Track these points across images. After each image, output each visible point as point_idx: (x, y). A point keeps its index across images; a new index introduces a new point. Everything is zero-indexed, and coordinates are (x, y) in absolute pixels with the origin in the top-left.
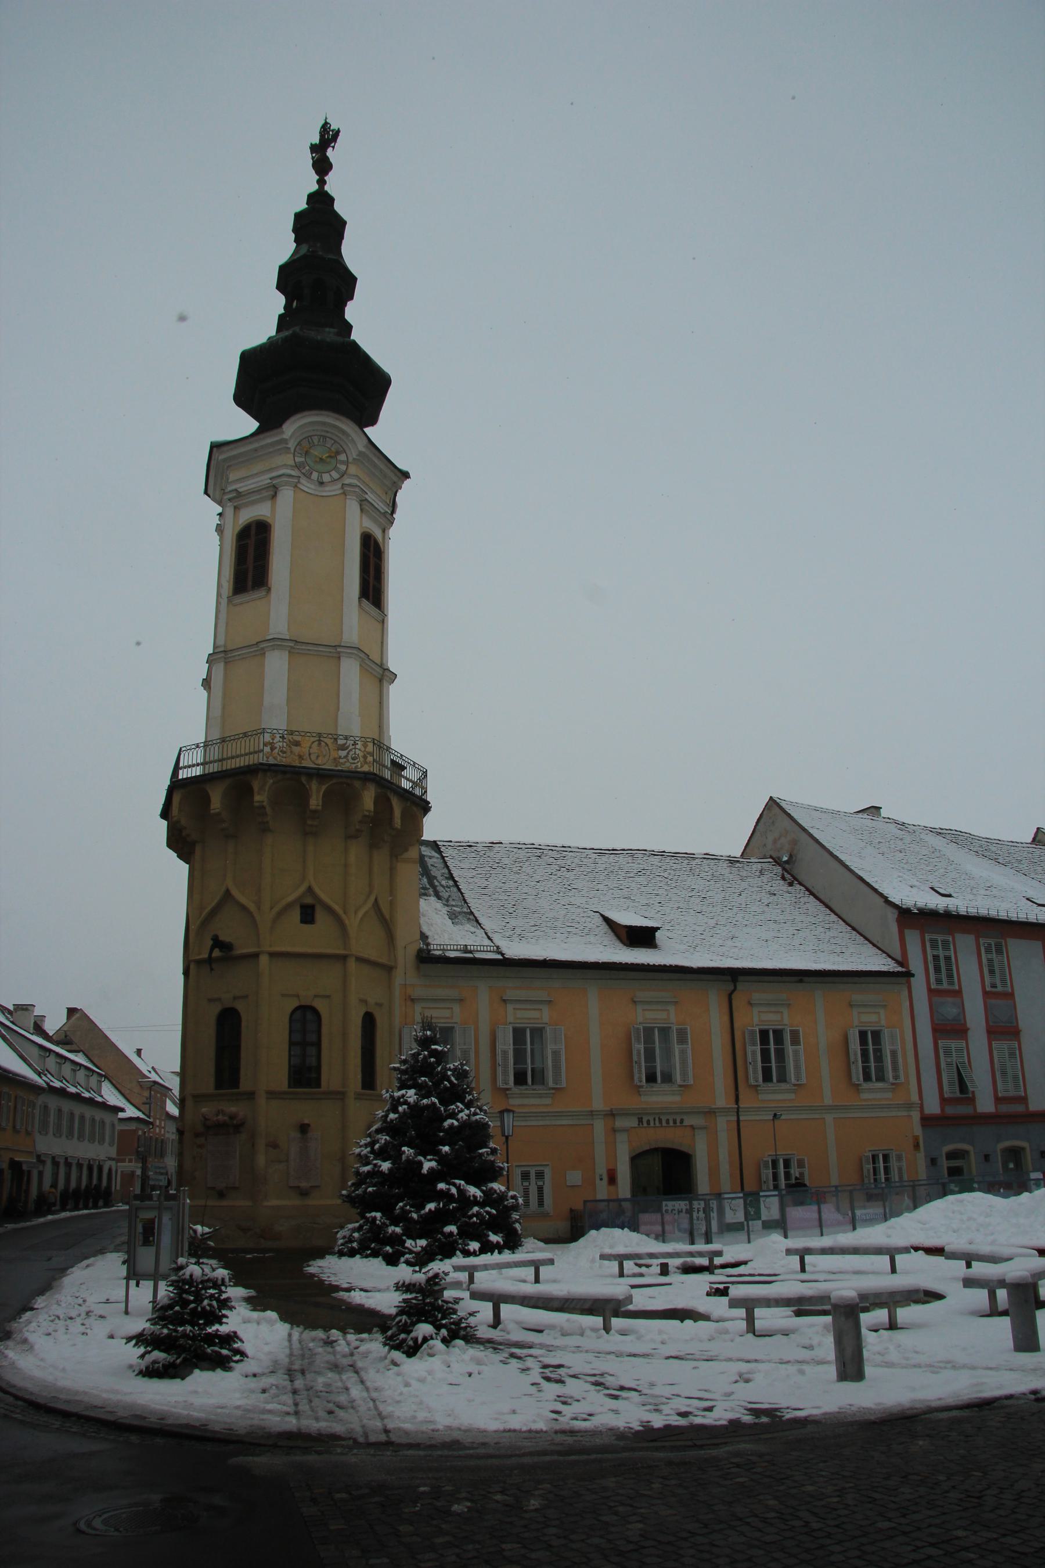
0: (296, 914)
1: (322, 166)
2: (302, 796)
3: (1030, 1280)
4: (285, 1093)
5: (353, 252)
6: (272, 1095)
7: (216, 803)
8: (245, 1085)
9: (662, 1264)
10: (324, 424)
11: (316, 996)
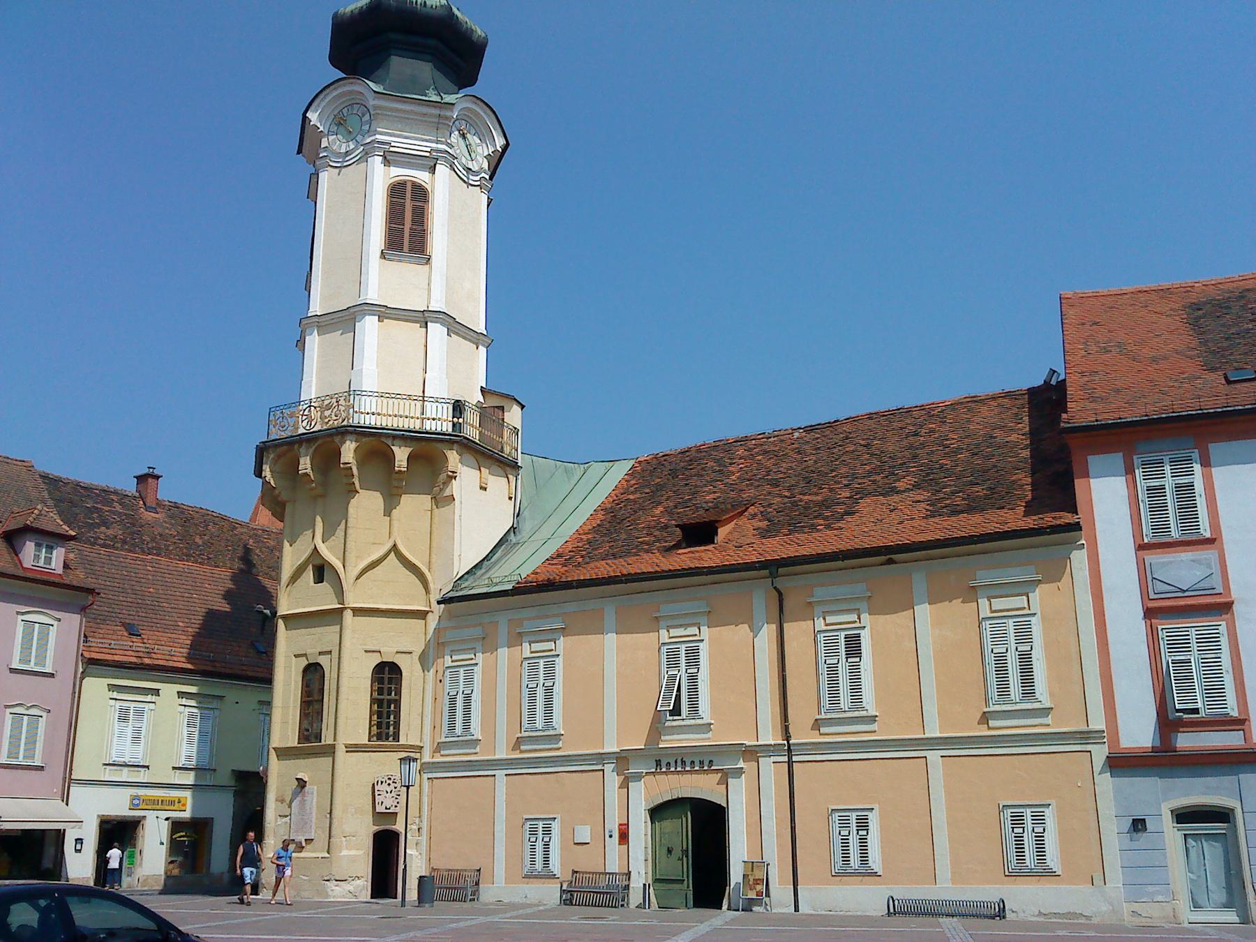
0: (309, 574)
3: (63, 874)
4: (365, 746)
6: (353, 749)
7: (305, 464)
8: (327, 739)
9: (257, 894)
10: (351, 92)
11: (320, 653)
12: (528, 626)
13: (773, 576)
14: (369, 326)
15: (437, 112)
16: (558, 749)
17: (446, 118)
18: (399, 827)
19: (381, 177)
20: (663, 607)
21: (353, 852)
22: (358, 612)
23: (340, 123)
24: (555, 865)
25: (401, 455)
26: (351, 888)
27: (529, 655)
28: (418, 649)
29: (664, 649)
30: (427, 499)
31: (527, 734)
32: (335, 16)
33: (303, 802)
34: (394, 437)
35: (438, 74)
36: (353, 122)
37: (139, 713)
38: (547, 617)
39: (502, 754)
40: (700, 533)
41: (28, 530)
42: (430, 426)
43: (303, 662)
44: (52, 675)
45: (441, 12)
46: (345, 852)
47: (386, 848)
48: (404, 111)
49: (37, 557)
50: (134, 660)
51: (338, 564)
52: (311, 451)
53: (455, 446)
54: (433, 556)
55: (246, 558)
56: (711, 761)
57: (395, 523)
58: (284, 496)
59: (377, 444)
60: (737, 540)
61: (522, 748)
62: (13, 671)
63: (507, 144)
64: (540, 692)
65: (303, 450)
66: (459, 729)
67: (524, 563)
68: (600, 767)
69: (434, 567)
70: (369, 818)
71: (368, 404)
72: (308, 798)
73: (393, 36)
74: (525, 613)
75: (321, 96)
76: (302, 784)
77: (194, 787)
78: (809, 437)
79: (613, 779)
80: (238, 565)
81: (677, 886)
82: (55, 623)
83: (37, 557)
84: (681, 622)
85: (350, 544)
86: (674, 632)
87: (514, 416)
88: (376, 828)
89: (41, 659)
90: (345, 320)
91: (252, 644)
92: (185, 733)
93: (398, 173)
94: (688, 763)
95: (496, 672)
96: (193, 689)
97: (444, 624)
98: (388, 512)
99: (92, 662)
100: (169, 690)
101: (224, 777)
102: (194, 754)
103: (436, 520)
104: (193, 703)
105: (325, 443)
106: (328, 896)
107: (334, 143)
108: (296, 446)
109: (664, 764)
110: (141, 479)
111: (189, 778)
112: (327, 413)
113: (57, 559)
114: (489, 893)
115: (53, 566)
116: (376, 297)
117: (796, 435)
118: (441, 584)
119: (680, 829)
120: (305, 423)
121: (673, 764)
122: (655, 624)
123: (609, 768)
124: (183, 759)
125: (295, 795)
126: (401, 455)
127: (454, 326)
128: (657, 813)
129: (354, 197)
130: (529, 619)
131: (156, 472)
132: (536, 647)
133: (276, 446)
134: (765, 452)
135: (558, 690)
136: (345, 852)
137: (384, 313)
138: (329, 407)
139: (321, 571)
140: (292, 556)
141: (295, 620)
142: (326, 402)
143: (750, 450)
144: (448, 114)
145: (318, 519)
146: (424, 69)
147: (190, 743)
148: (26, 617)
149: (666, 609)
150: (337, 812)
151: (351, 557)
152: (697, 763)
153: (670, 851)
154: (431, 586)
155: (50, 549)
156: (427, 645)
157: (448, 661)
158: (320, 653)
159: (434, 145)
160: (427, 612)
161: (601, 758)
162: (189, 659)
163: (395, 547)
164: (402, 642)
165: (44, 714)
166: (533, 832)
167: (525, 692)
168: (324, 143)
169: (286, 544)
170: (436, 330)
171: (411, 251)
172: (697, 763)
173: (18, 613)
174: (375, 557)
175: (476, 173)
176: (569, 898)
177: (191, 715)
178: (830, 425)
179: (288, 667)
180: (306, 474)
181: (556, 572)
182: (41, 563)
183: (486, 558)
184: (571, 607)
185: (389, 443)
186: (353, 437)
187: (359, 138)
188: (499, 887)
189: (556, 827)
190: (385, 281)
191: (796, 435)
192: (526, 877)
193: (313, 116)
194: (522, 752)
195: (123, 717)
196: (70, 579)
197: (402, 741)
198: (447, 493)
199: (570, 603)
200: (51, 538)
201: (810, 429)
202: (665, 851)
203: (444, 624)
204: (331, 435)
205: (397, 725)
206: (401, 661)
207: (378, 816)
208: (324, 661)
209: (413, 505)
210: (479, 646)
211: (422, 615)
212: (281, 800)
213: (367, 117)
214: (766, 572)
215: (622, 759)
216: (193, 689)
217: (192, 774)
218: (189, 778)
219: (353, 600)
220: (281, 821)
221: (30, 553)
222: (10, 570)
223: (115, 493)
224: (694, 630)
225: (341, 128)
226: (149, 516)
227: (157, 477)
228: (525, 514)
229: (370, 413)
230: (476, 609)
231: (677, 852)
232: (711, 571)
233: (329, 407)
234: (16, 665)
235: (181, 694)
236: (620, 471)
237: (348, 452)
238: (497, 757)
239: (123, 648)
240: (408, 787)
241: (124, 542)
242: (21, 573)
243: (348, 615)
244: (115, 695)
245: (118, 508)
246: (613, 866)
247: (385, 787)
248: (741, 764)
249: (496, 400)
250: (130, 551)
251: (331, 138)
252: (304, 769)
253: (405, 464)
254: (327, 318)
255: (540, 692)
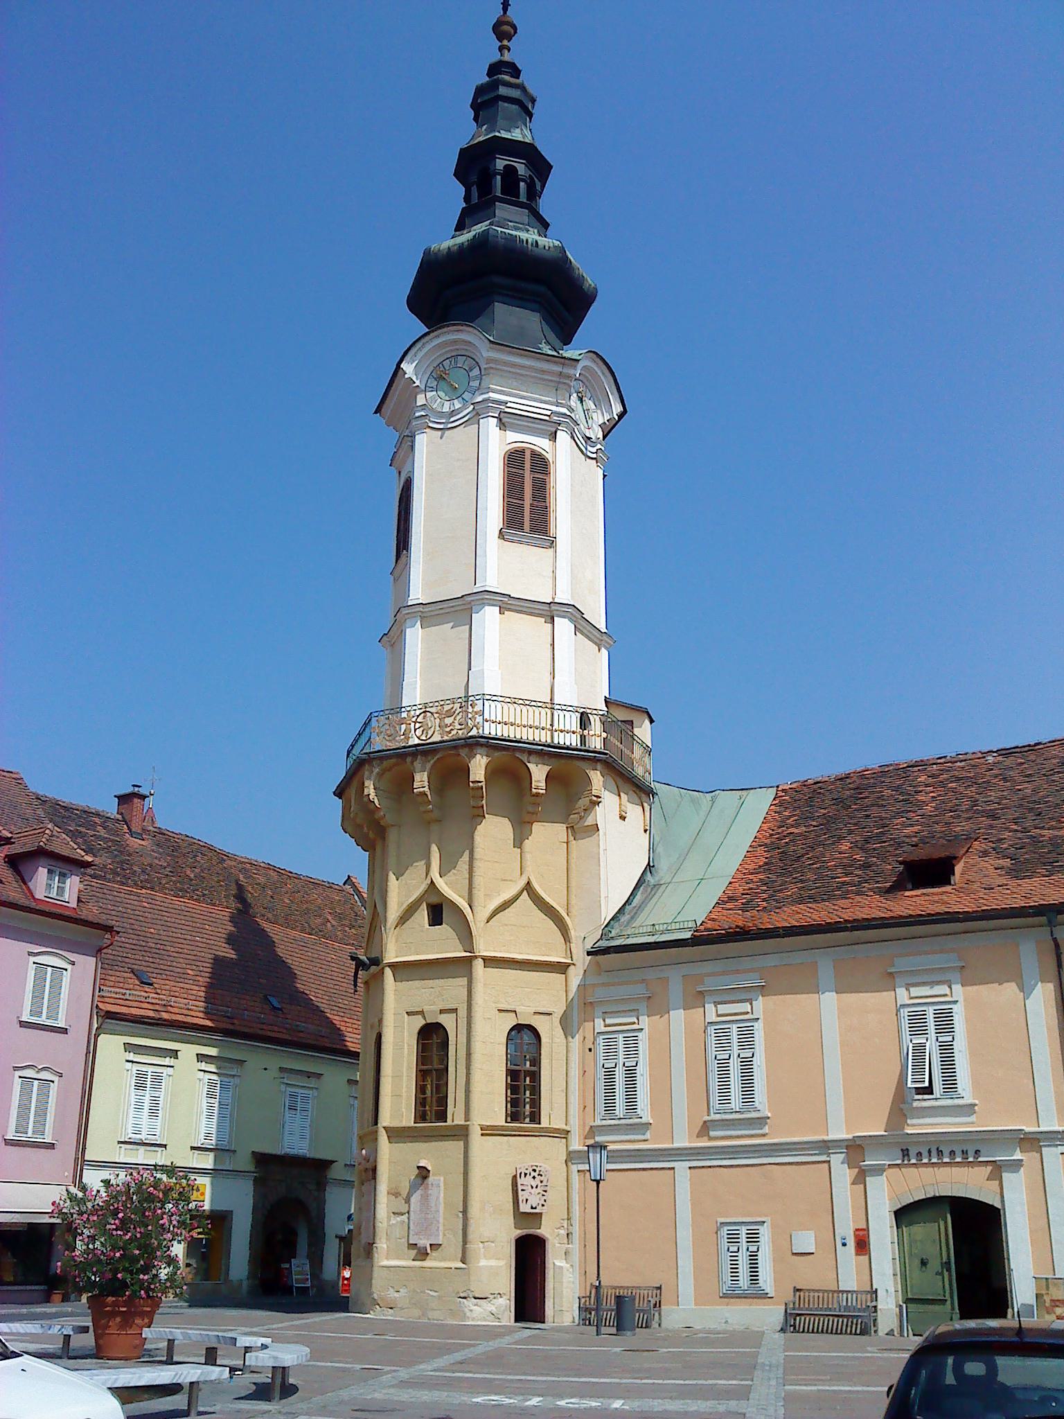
0: (423, 915)
1: (503, 31)
2: (519, 778)
5: (472, 114)
7: (421, 781)
8: (455, 1116)
10: (455, 342)
11: (442, 1012)
12: (710, 984)
13: (1051, 924)
14: (488, 617)
15: (558, 369)
16: (764, 1135)
17: (569, 377)
18: (544, 1231)
19: (496, 442)
20: (897, 961)
21: (493, 1263)
22: (490, 962)
23: (440, 377)
24: (766, 1279)
25: (539, 773)
26: (493, 1309)
27: (715, 1019)
28: (559, 1009)
29: (905, 1012)
30: (561, 828)
31: (718, 1117)
32: (427, 253)
33: (425, 1198)
34: (530, 752)
35: (546, 327)
36: (457, 378)
37: (157, 1079)
38: (737, 972)
39: (682, 1142)
40: (931, 871)
41: (41, 854)
42: (561, 739)
43: (419, 1022)
44: (64, 1031)
45: (556, 254)
46: (483, 1263)
47: (530, 1255)
48: (523, 367)
49: (49, 886)
50: (151, 1014)
51: (462, 903)
52: (429, 766)
53: (599, 766)
54: (573, 897)
55: (240, 896)
56: (977, 1152)
57: (528, 857)
58: (389, 819)
59: (510, 758)
60: (979, 880)
61: (712, 1133)
62: (23, 1024)
63: (625, 412)
64: (735, 1068)
65: (417, 764)
66: (620, 1109)
67: (687, 905)
68: (824, 1158)
69: (574, 911)
70: (510, 1220)
71: (493, 711)
72: (432, 1191)
73: (497, 279)
74: (708, 967)
75: (419, 345)
76: (423, 1173)
77: (214, 1172)
78: (1009, 761)
79: (842, 1173)
80: (233, 904)
81: (937, 1308)
82: (69, 967)
83: (49, 886)
84: (926, 978)
85: (478, 880)
86: (915, 991)
87: (644, 731)
88: (519, 1233)
89: (53, 1014)
90: (459, 610)
91: (265, 996)
92: (205, 1105)
93: (514, 438)
94: (946, 1152)
95: (670, 1044)
96: (213, 1052)
97: (591, 980)
98: (519, 843)
99: (110, 1015)
100: (188, 1051)
101: (244, 1162)
102: (214, 1131)
103: (574, 855)
104: (212, 1068)
105: (448, 758)
106: (465, 1317)
107: (432, 400)
108: (409, 759)
109: (913, 1152)
110: (124, 799)
111: (208, 1161)
112: (448, 721)
113: (70, 890)
114: (675, 1316)
115: (66, 898)
116: (495, 583)
117: (990, 759)
118: (585, 933)
119: (936, 1236)
120: (419, 732)
121: (925, 1153)
122: (889, 980)
123: (837, 1159)
124: (202, 1136)
125: (413, 1188)
126: (539, 773)
127: (581, 624)
128: (904, 1215)
129: (460, 468)
130: (709, 975)
131: (142, 791)
132: (723, 1009)
133: (381, 759)
134: (958, 779)
135: (759, 1063)
136: (483, 1263)
137: (507, 603)
138: (450, 714)
139: (438, 912)
140: (400, 892)
141: (404, 970)
142: (447, 708)
143: (933, 776)
144: (571, 372)
145: (434, 848)
146: (531, 321)
147: (210, 1117)
148: (40, 959)
149: (902, 964)
150: (474, 1210)
151: (479, 894)
152: (958, 1153)
153: (924, 1263)
154: (573, 933)
155: (63, 876)
156: (569, 1006)
157: (599, 1025)
158: (442, 1012)
159: (554, 408)
160: (568, 965)
161: (825, 1146)
162: (207, 1014)
163: (528, 887)
164: (541, 1000)
165: (56, 1079)
166: (733, 1238)
167: (713, 1066)
168: (421, 400)
169: (392, 877)
170: (564, 626)
171: (532, 530)
172: (958, 1153)
173: (30, 954)
174: (507, 895)
175: (594, 444)
176: (793, 1322)
177: (211, 1084)
178: (1032, 748)
179: (398, 1027)
180: (424, 794)
181: (735, 918)
182: (53, 895)
183: (628, 902)
184: (771, 961)
185: (524, 758)
186: (483, 750)
187: (466, 396)
188: (687, 1309)
189: (765, 1233)
190: (506, 565)
191: (990, 759)
192: (725, 1296)
193: (408, 368)
194: (711, 1139)
195: (140, 1086)
196: (84, 914)
197: (545, 1123)
198: (589, 821)
199: (770, 956)
200: (66, 864)
201: (1006, 752)
202: (917, 1262)
203: (591, 980)
204: (455, 747)
205: (536, 1103)
206: (541, 1025)
207: (522, 1218)
208: (447, 1021)
209: (547, 835)
210: (643, 1007)
211: (562, 968)
212: (394, 1193)
213: (476, 372)
214: (1044, 919)
215: (855, 1149)
216: (213, 1052)
217: (212, 1155)
218: (208, 1161)
219: (484, 948)
220: (396, 1220)
221: (43, 884)
222: (23, 901)
223: (98, 815)
224: (943, 989)
225: (443, 383)
226: (135, 843)
227: (143, 797)
228: (660, 849)
229: (496, 722)
230: (629, 963)
231: (935, 1265)
232: (968, 917)
233: (450, 714)
234: (25, 1018)
235: (201, 1057)
236: (760, 804)
237: (478, 767)
238: (676, 1145)
239: (138, 1001)
240: (598, 1182)
241: (116, 874)
242: (33, 905)
243: (478, 965)
244: (131, 1056)
245: (102, 833)
246: (850, 1279)
247: (528, 1181)
248: (1018, 1156)
249: (621, 713)
250: (123, 884)
251: (429, 395)
252: (426, 1154)
253: (543, 785)
254: (433, 607)
255: (735, 1068)
